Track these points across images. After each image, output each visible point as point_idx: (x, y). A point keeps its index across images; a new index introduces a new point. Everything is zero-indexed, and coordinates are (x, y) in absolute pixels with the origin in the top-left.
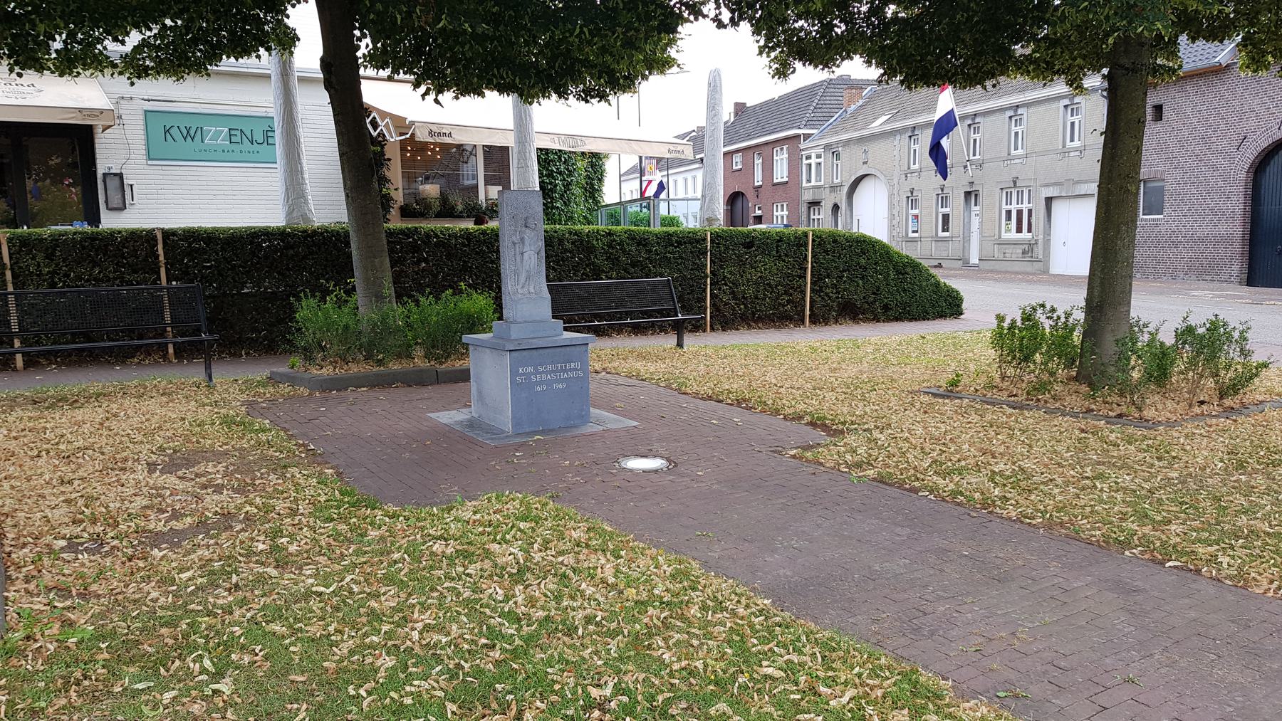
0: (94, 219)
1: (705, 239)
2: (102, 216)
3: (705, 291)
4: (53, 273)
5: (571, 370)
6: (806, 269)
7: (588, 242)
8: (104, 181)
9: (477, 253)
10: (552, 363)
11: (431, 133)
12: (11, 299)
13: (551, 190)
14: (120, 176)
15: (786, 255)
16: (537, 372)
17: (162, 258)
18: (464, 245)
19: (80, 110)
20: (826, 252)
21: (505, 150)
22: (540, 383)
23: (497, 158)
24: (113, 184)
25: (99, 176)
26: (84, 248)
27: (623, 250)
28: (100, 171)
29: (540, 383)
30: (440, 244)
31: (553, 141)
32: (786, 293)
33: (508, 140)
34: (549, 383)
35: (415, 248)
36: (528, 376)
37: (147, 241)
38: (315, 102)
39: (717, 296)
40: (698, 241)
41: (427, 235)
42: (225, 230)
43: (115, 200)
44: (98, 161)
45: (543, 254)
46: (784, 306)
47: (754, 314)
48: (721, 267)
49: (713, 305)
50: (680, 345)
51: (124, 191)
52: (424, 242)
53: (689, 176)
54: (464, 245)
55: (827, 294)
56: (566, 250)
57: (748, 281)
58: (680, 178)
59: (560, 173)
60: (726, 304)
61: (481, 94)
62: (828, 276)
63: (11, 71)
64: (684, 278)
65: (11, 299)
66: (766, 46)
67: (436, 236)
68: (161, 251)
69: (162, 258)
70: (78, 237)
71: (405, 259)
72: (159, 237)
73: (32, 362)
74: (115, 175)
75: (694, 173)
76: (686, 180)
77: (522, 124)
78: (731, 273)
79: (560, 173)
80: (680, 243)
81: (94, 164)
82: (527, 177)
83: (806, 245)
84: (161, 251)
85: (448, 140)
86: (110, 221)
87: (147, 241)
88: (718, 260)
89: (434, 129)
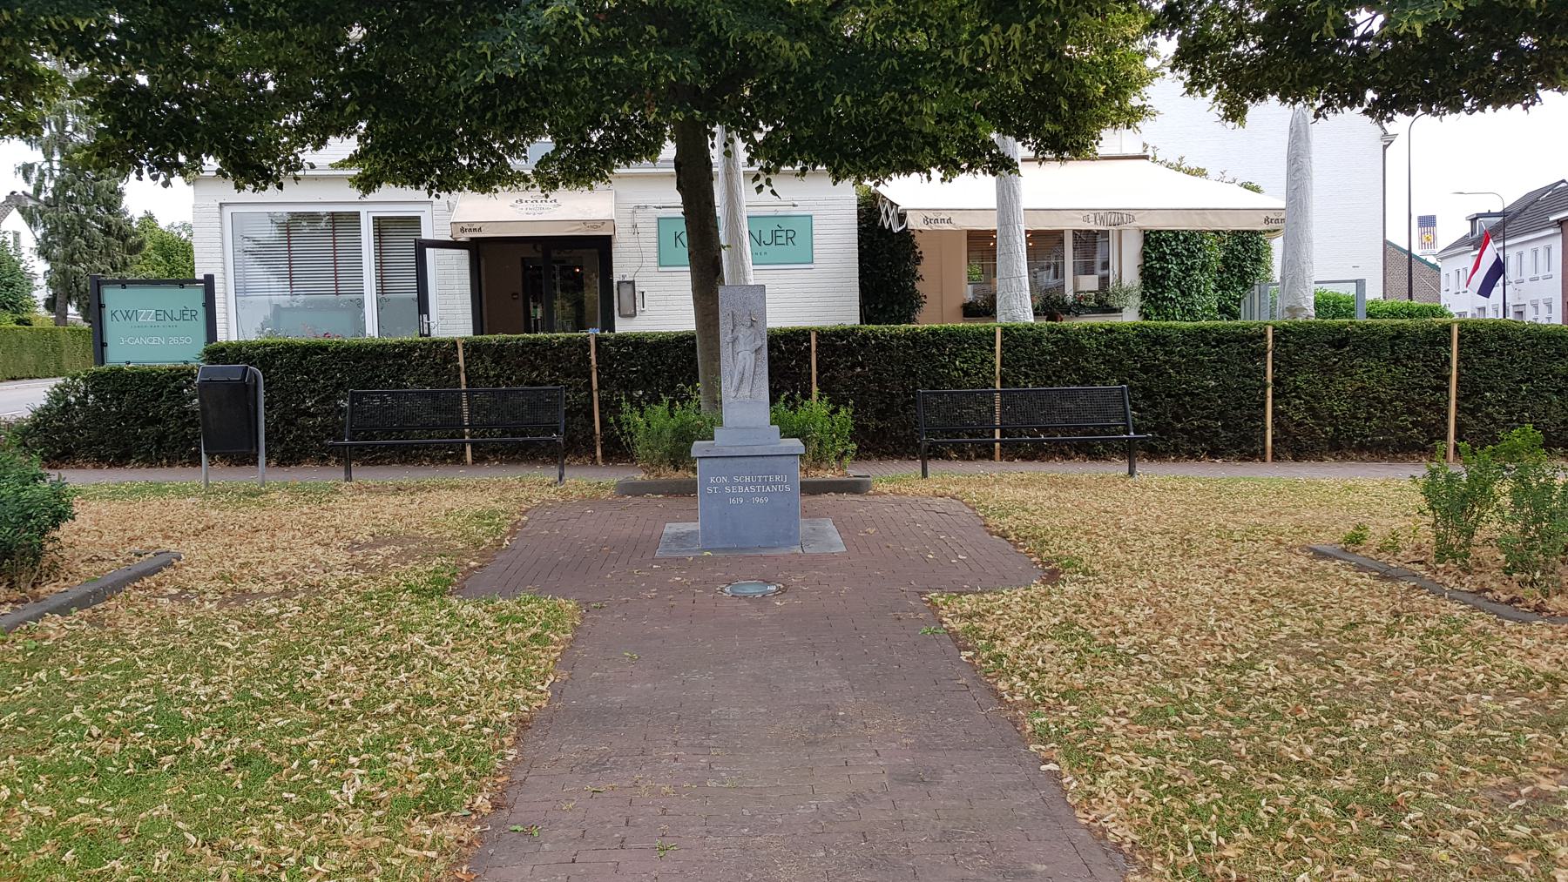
1: (1263, 336)
3: (1263, 405)
4: (498, 376)
6: (1447, 379)
7: (1076, 341)
10: (751, 474)
11: (927, 221)
12: (464, 396)
13: (1163, 277)
14: (633, 283)
15: (1409, 358)
19: (585, 222)
20: (1488, 353)
21: (988, 236)
22: (736, 496)
23: (982, 245)
24: (626, 291)
27: (1130, 352)
28: (616, 279)
29: (736, 496)
31: (1086, 219)
32: (1411, 412)
33: (989, 223)
35: (849, 351)
39: (1283, 413)
40: (1251, 339)
46: (1405, 429)
47: (1350, 439)
48: (1290, 373)
49: (1276, 425)
50: (1131, 473)
53: (1541, 246)
55: (1488, 415)
56: (1043, 353)
57: (1338, 393)
58: (1527, 251)
59: (1177, 255)
60: (1299, 425)
62: (1491, 389)
63: (430, 194)
64: (1228, 389)
65: (464, 396)
66: (1193, 84)
67: (876, 338)
68: (593, 357)
71: (838, 364)
73: (479, 459)
75: (1546, 243)
76: (1536, 251)
77: (1006, 199)
78: (1307, 381)
79: (1177, 255)
80: (1219, 342)
81: (611, 273)
82: (1127, 267)
83: (1448, 343)
84: (593, 357)
86: (622, 327)
88: (1286, 365)
89: (931, 215)
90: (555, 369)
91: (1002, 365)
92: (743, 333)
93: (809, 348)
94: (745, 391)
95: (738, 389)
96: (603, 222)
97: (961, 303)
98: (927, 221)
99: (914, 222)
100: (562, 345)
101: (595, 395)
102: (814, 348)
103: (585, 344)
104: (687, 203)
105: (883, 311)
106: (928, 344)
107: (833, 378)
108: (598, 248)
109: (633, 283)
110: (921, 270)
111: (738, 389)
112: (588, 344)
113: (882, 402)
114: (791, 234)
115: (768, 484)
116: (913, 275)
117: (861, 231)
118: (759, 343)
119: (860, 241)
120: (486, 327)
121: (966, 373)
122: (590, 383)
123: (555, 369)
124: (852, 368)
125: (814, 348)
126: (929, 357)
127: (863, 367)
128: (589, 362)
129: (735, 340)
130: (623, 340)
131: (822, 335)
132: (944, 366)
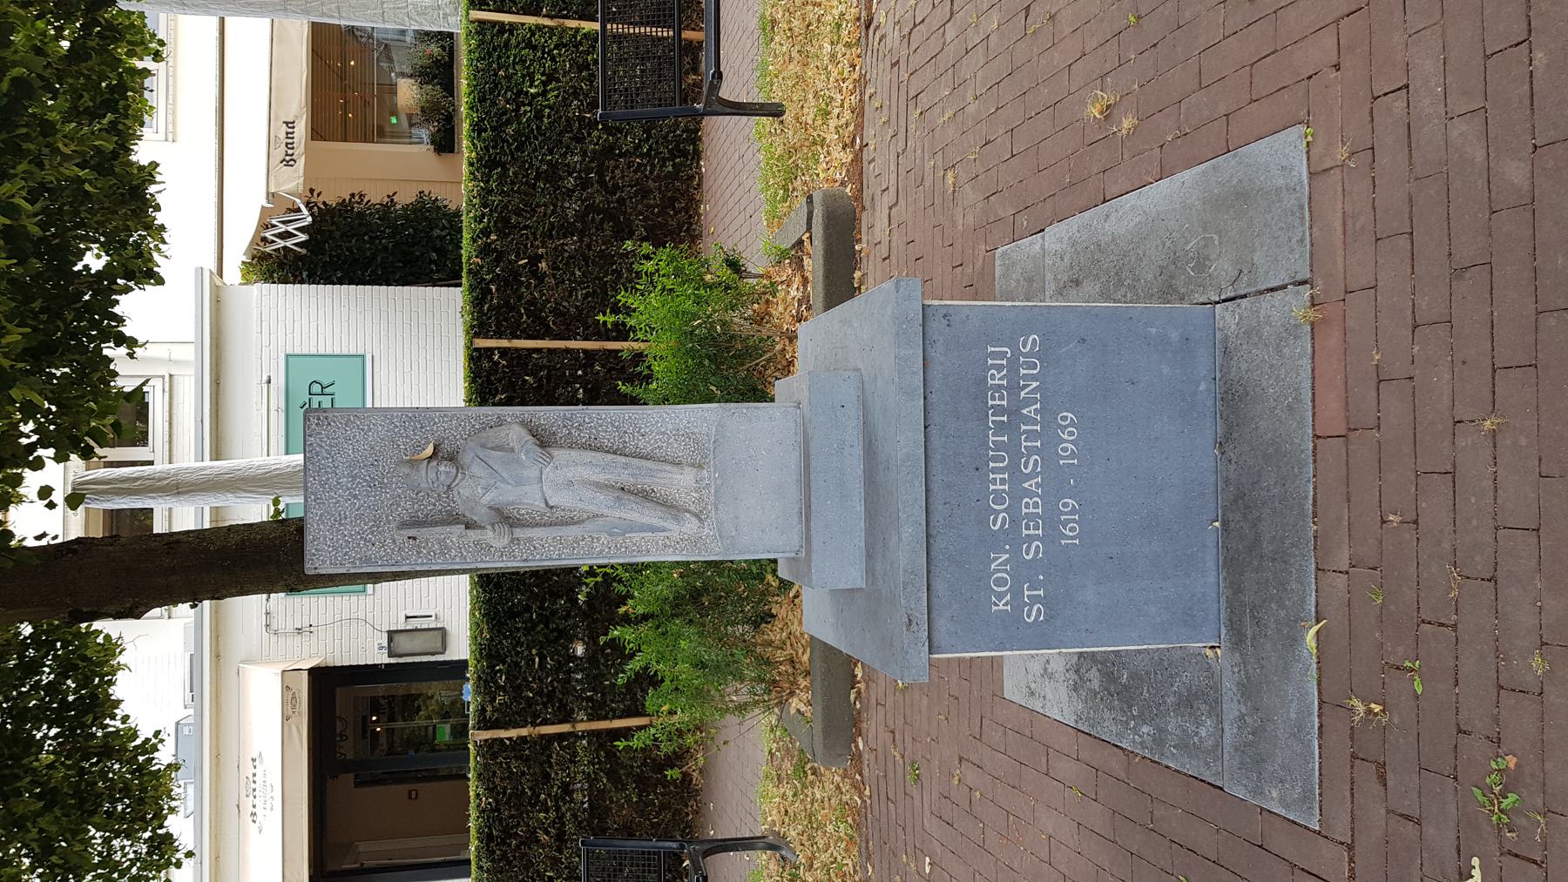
0: (456, 669)
2: (456, 658)
5: (1014, 388)
8: (400, 656)
9: (520, 148)
11: (288, 161)
14: (391, 634)
16: (1013, 536)
17: (524, 732)
18: (503, 175)
19: (285, 718)
22: (1052, 522)
24: (404, 644)
25: (393, 661)
26: (504, 856)
28: (383, 659)
29: (1052, 522)
30: (504, 226)
34: (1055, 486)
35: (510, 280)
36: (1022, 572)
37: (494, 756)
38: (255, 327)
41: (484, 251)
42: (476, 626)
43: (432, 642)
44: (370, 662)
45: (546, 415)
51: (416, 630)
52: (497, 261)
54: (503, 175)
61: (148, 173)
67: (485, 232)
68: (513, 733)
69: (524, 732)
70: (486, 865)
71: (532, 302)
72: (482, 343)
74: (390, 640)
84: (513, 733)
85: (301, 130)
86: (461, 648)
87: (494, 756)
89: (280, 153)
90: (534, 801)
91: (537, 13)
92: (478, 488)
93: (504, 352)
94: (678, 483)
95: (672, 508)
96: (286, 688)
97: (432, 155)
98: (288, 161)
99: (292, 181)
100: (490, 790)
101: (581, 727)
102: (504, 343)
103: (492, 749)
104: (169, 596)
105: (442, 252)
106: (498, 140)
107: (556, 312)
108: (328, 686)
109: (391, 634)
110: (376, 196)
111: (672, 508)
112: (489, 744)
113: (600, 227)
114: (316, 389)
115: (1014, 412)
116: (387, 208)
117: (313, 279)
118: (515, 435)
119: (329, 281)
120: (461, 857)
121: (550, 77)
122: (560, 737)
123: (534, 801)
124: (540, 278)
125: (504, 343)
126: (522, 140)
127: (539, 258)
128: (523, 739)
129: (507, 519)
130: (489, 652)
131: (479, 327)
132: (539, 116)
